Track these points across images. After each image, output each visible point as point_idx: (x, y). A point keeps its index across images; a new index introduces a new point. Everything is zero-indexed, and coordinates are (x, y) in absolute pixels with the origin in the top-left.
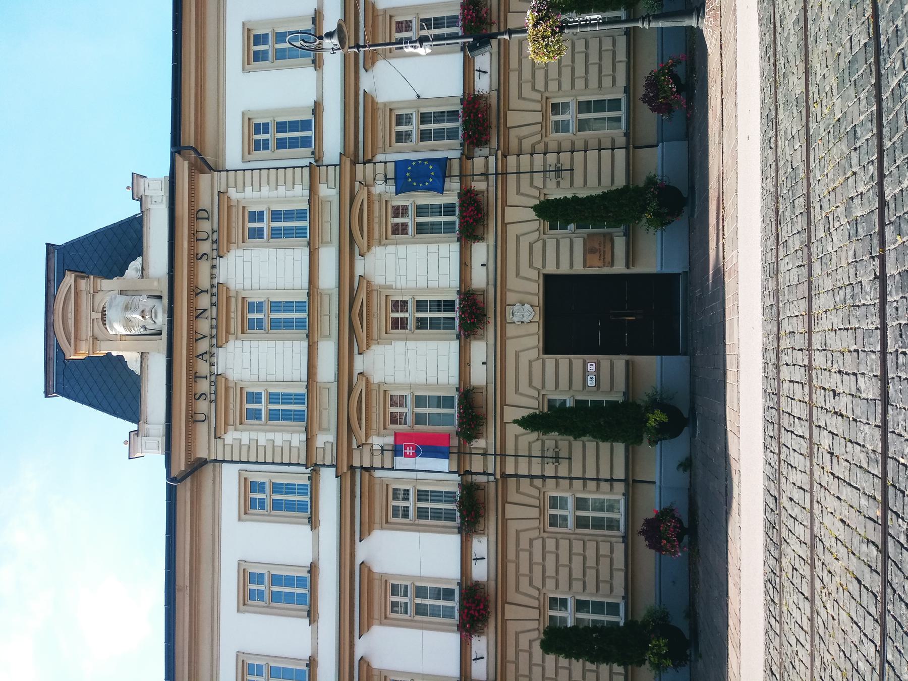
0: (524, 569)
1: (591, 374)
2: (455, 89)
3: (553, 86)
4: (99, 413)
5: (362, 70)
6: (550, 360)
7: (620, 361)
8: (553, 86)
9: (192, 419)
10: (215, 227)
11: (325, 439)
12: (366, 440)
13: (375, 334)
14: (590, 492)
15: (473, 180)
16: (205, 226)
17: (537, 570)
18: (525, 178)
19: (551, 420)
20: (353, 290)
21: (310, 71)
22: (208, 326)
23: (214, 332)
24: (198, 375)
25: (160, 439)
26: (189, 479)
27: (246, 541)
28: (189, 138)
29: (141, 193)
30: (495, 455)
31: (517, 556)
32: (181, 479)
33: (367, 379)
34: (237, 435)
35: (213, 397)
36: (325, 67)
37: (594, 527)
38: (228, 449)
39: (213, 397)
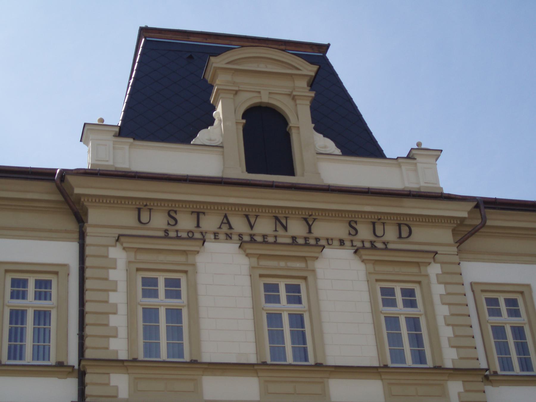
26: (60, 198)
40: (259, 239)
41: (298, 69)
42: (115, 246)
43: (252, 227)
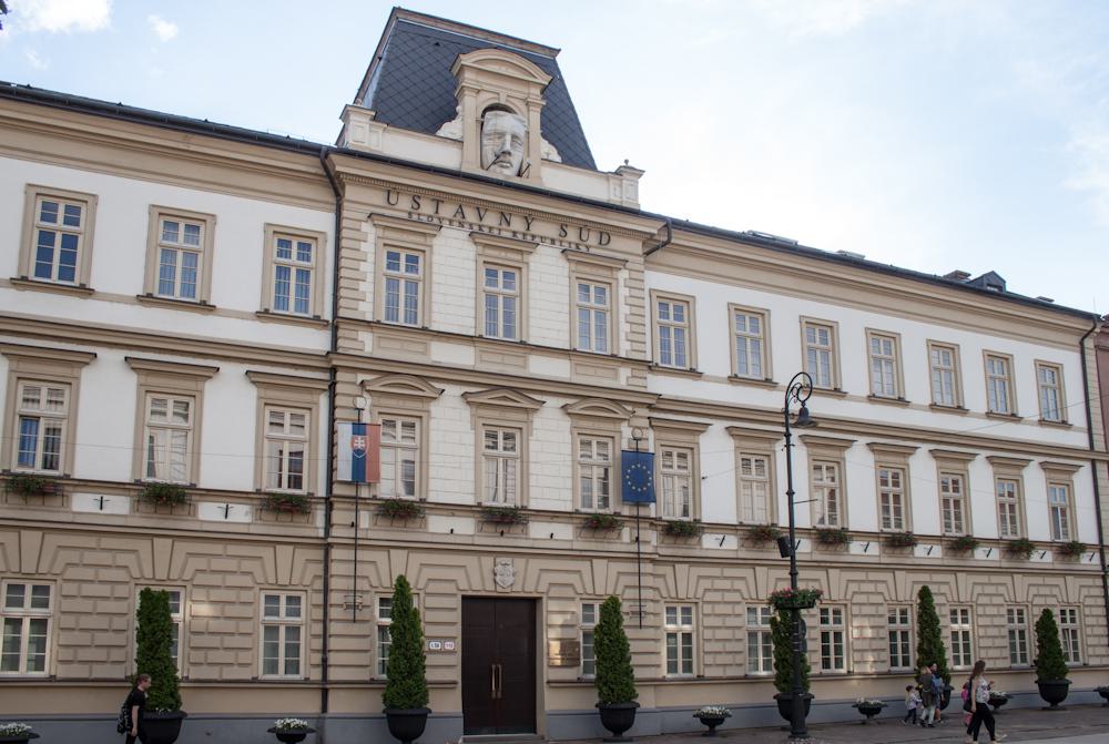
0: (217, 564)
1: (443, 645)
3: (70, 589)
4: (580, 117)
6: (457, 603)
7: (455, 675)
8: (70, 589)
9: (392, 189)
10: (592, 251)
11: (366, 343)
12: (368, 391)
13: (482, 412)
14: (372, 644)
15: (632, 528)
16: (593, 239)
17: (89, 574)
18: (634, 581)
19: (400, 602)
20: (430, 378)
21: (138, 289)
22: (490, 224)
23: (486, 230)
24: (440, 204)
25: (366, 145)
26: (321, 171)
27: (242, 227)
28: (679, 238)
29: (625, 175)
30: (356, 538)
31: (726, 578)
33: (435, 398)
34: (371, 238)
35: (415, 217)
36: (730, 386)
37: (690, 657)
38: (356, 225)
39: (415, 217)
42: (366, 222)
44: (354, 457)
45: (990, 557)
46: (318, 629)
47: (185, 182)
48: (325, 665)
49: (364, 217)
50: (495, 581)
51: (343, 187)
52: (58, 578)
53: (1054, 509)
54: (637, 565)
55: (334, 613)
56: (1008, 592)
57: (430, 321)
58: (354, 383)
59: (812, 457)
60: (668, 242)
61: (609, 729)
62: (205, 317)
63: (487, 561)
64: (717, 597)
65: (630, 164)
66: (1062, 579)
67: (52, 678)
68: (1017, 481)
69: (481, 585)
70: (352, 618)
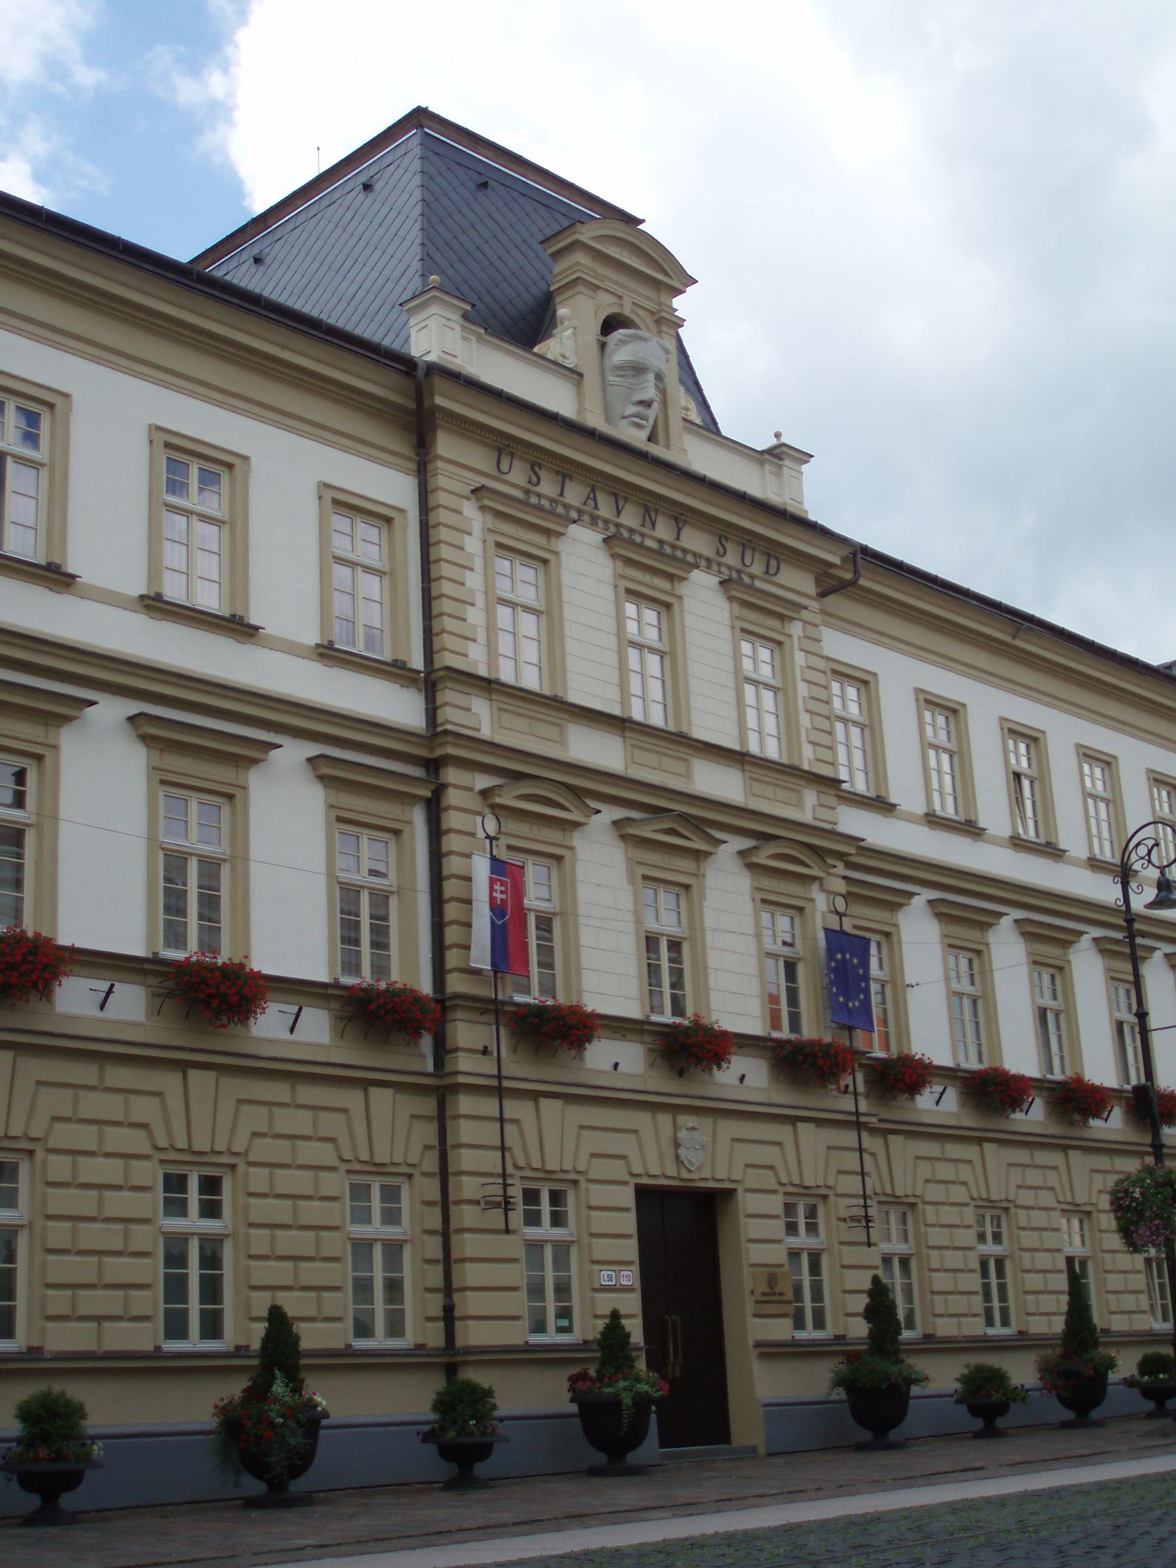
2: (73, 930)
3: (59, 1167)
5: (135, 707)
6: (627, 1196)
8: (59, 1167)
10: (758, 584)
24: (567, 481)
26: (412, 405)
30: (857, 1114)
32: (420, 394)
40: (600, 523)
41: (667, 275)
42: (468, 499)
43: (619, 512)
44: (493, 922)
45: (111, 1012)
46: (434, 1247)
47: (1018, 688)
48: (449, 1316)
49: (466, 490)
50: (677, 1157)
51: (434, 429)
52: (581, 1178)
53: (651, 942)
54: (496, 1101)
55: (467, 1216)
56: (975, 1178)
57: (565, 687)
58: (471, 789)
59: (335, 813)
60: (853, 583)
61: (601, 1449)
62: (886, 820)
63: (665, 1120)
64: (86, 1137)
65: (784, 440)
66: (788, 1129)
67: (34, 1353)
68: (1060, 969)
69: (660, 1169)
70: (865, 1239)
